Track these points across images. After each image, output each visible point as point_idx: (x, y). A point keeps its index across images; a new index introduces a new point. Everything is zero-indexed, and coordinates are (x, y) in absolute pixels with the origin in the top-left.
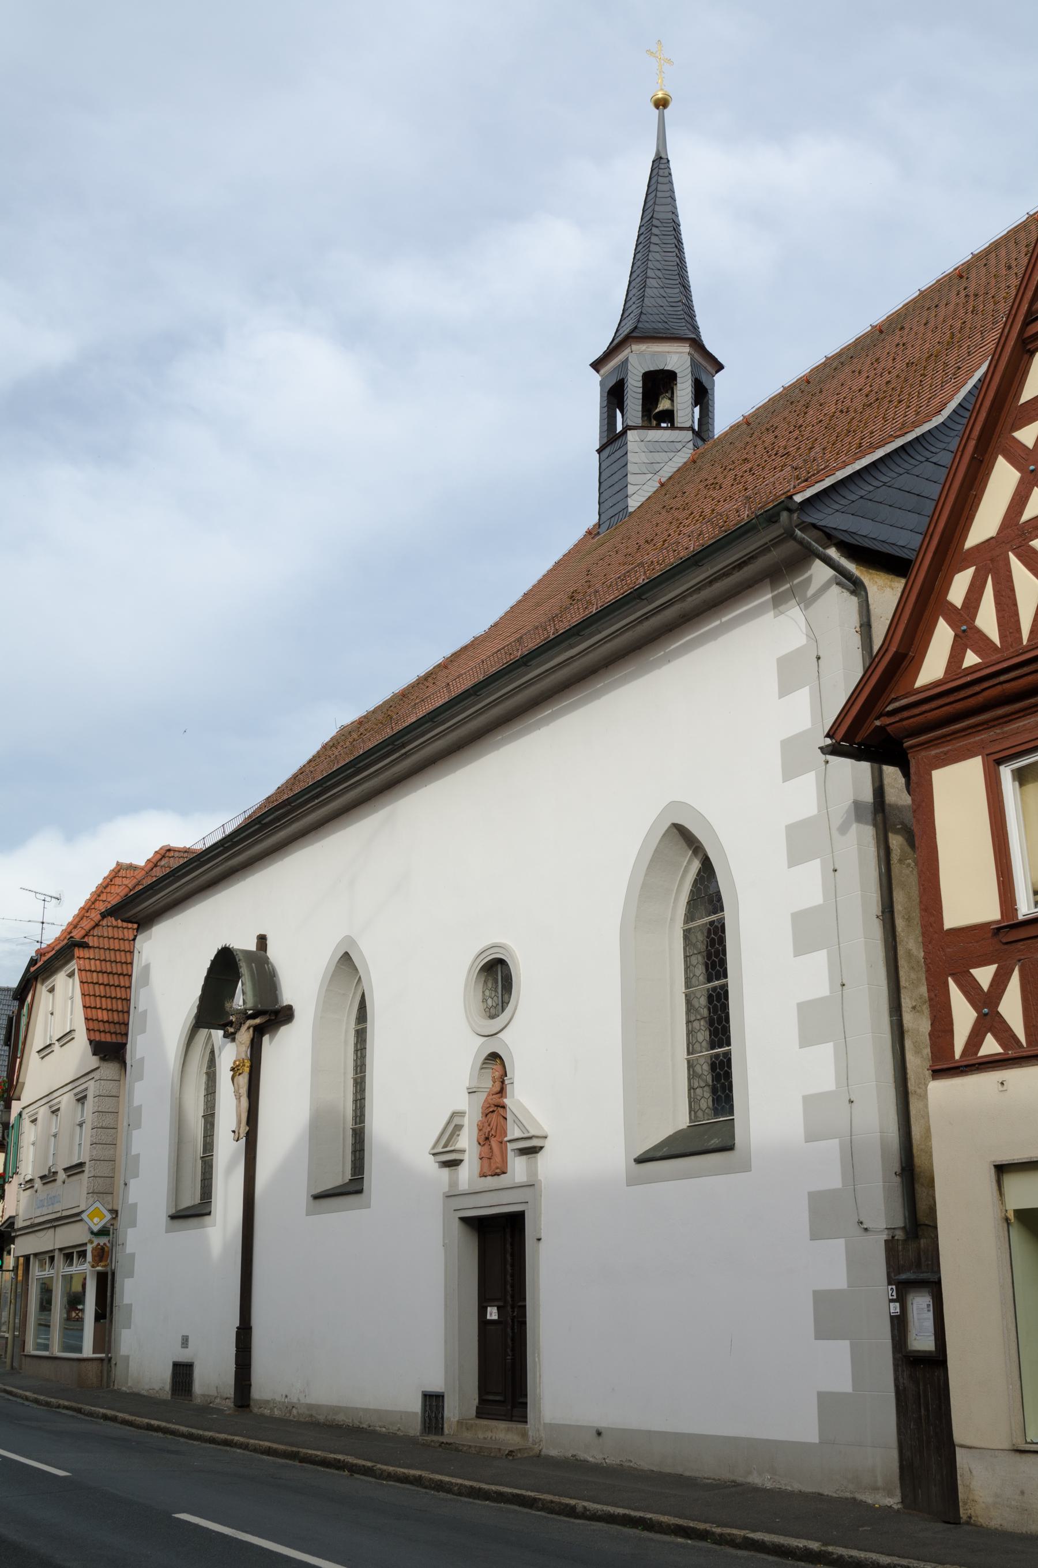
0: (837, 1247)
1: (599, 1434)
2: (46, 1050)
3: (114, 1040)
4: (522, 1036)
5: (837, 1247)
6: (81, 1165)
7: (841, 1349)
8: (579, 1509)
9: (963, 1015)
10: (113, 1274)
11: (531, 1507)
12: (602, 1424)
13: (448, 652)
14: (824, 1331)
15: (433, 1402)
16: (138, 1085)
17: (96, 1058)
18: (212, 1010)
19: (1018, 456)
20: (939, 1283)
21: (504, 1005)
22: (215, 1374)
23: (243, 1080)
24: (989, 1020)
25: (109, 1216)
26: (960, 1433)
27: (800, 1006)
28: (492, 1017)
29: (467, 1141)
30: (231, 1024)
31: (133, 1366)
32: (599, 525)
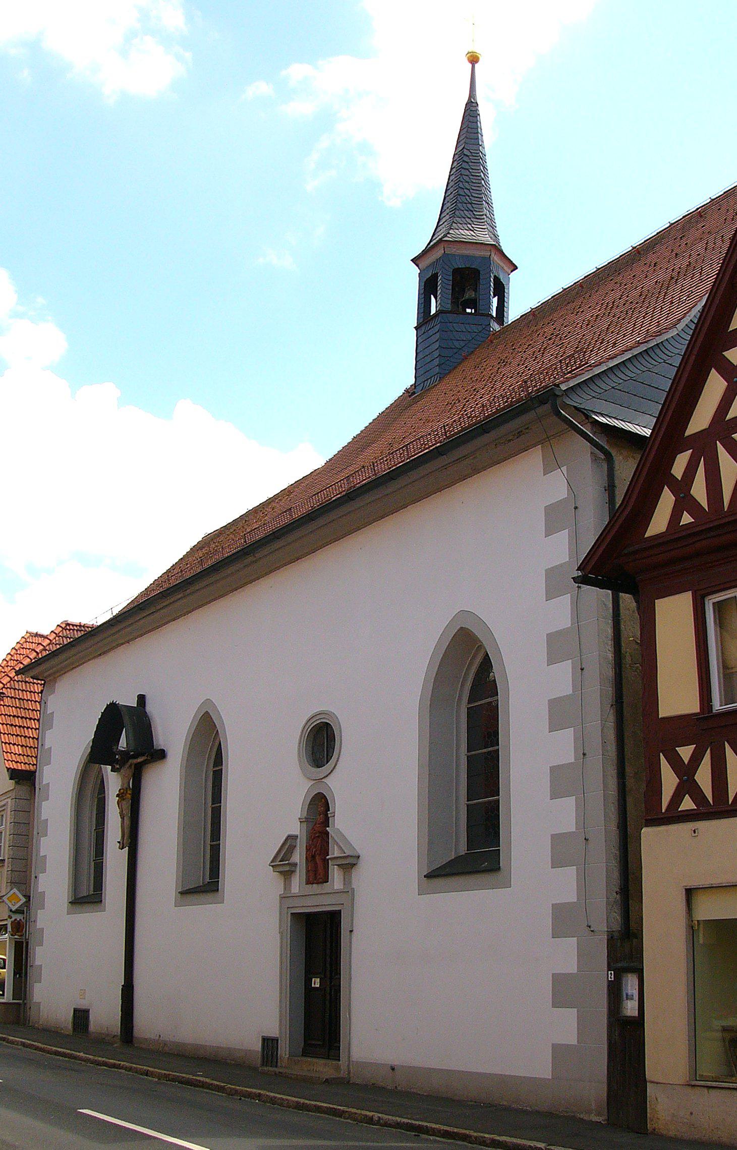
0: (571, 943)
1: (393, 1069)
3: (23, 768)
4: (341, 783)
5: (571, 943)
7: (571, 1014)
8: (376, 1118)
9: (669, 780)
10: (27, 943)
11: (340, 1116)
12: (396, 1063)
14: (558, 1002)
15: (269, 1044)
16: (44, 804)
18: (102, 750)
19: (725, 369)
20: (642, 969)
22: (106, 1015)
23: (127, 805)
24: (687, 785)
25: (24, 900)
26: (650, 1073)
27: (553, 769)
28: (319, 766)
29: (298, 857)
30: (117, 761)
32: (415, 386)
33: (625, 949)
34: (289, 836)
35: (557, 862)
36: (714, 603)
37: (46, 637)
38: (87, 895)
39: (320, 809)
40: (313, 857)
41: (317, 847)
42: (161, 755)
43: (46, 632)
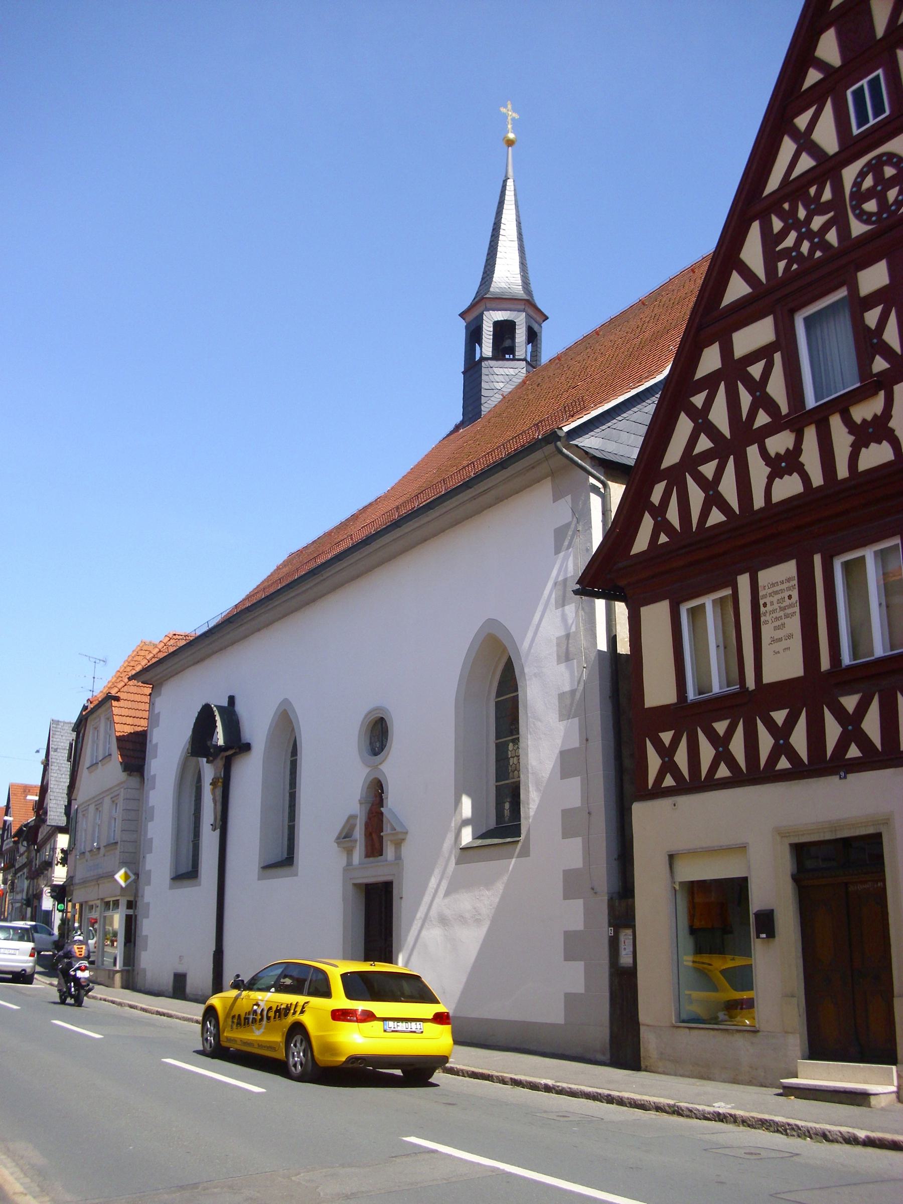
2: (94, 765)
4: (394, 767)
6: (116, 843)
7: (580, 966)
9: (654, 761)
10: (136, 916)
13: (353, 510)
17: (125, 773)
18: (200, 741)
21: (382, 747)
23: (219, 792)
24: (669, 766)
26: (643, 1017)
29: (359, 833)
31: (149, 975)
33: (622, 911)
34: (417, 978)
35: (567, 833)
36: (688, 610)
37: (155, 646)
38: (187, 874)
39: (377, 792)
40: (371, 834)
41: (374, 827)
42: (247, 747)
43: (157, 642)
